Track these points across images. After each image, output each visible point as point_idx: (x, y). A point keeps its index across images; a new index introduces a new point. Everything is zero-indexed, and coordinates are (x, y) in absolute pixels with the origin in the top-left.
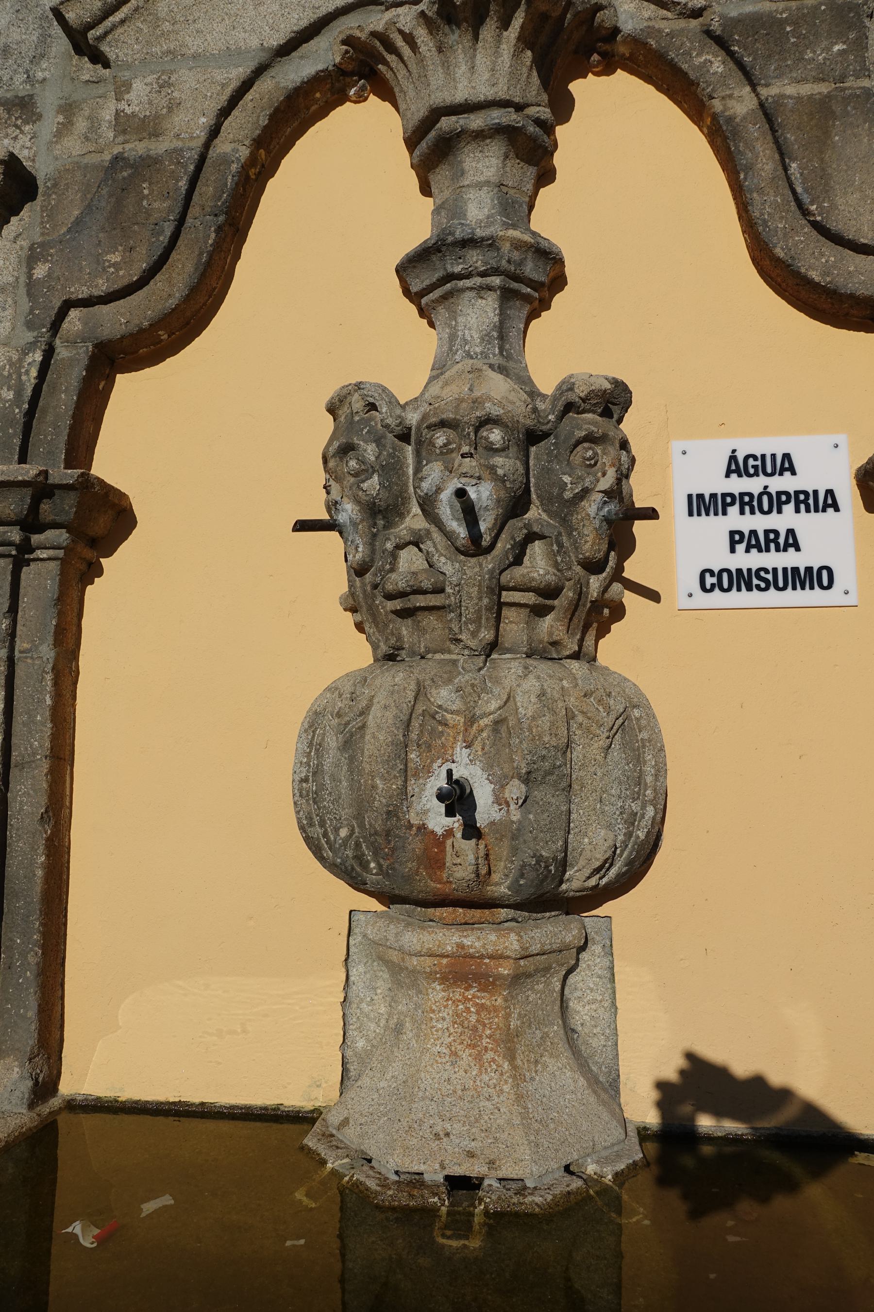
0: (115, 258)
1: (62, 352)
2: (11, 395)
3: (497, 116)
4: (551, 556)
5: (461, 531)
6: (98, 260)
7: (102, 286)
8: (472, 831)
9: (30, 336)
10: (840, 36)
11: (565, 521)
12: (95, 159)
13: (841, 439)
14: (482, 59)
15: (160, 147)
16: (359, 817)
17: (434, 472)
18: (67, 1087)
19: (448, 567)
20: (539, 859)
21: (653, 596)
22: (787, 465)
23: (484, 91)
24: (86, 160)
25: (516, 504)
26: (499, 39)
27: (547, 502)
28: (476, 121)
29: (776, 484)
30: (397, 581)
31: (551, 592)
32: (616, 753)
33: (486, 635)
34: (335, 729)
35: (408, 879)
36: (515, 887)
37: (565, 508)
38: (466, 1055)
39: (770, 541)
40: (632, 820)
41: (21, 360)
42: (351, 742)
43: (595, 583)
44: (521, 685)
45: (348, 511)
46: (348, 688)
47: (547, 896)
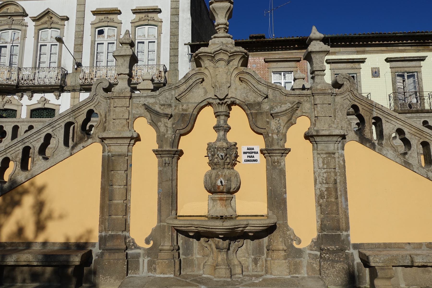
1: (176, 135)
3: (224, 113)
7: (181, 128)
8: (222, 185)
14: (222, 107)
15: (187, 113)
16: (211, 184)
17: (219, 152)
18: (178, 214)
29: (252, 151)
30: (215, 162)
31: (229, 163)
34: (208, 176)
37: (231, 155)
39: (251, 157)
42: (210, 177)
43: (234, 162)
44: (227, 172)
45: (210, 155)
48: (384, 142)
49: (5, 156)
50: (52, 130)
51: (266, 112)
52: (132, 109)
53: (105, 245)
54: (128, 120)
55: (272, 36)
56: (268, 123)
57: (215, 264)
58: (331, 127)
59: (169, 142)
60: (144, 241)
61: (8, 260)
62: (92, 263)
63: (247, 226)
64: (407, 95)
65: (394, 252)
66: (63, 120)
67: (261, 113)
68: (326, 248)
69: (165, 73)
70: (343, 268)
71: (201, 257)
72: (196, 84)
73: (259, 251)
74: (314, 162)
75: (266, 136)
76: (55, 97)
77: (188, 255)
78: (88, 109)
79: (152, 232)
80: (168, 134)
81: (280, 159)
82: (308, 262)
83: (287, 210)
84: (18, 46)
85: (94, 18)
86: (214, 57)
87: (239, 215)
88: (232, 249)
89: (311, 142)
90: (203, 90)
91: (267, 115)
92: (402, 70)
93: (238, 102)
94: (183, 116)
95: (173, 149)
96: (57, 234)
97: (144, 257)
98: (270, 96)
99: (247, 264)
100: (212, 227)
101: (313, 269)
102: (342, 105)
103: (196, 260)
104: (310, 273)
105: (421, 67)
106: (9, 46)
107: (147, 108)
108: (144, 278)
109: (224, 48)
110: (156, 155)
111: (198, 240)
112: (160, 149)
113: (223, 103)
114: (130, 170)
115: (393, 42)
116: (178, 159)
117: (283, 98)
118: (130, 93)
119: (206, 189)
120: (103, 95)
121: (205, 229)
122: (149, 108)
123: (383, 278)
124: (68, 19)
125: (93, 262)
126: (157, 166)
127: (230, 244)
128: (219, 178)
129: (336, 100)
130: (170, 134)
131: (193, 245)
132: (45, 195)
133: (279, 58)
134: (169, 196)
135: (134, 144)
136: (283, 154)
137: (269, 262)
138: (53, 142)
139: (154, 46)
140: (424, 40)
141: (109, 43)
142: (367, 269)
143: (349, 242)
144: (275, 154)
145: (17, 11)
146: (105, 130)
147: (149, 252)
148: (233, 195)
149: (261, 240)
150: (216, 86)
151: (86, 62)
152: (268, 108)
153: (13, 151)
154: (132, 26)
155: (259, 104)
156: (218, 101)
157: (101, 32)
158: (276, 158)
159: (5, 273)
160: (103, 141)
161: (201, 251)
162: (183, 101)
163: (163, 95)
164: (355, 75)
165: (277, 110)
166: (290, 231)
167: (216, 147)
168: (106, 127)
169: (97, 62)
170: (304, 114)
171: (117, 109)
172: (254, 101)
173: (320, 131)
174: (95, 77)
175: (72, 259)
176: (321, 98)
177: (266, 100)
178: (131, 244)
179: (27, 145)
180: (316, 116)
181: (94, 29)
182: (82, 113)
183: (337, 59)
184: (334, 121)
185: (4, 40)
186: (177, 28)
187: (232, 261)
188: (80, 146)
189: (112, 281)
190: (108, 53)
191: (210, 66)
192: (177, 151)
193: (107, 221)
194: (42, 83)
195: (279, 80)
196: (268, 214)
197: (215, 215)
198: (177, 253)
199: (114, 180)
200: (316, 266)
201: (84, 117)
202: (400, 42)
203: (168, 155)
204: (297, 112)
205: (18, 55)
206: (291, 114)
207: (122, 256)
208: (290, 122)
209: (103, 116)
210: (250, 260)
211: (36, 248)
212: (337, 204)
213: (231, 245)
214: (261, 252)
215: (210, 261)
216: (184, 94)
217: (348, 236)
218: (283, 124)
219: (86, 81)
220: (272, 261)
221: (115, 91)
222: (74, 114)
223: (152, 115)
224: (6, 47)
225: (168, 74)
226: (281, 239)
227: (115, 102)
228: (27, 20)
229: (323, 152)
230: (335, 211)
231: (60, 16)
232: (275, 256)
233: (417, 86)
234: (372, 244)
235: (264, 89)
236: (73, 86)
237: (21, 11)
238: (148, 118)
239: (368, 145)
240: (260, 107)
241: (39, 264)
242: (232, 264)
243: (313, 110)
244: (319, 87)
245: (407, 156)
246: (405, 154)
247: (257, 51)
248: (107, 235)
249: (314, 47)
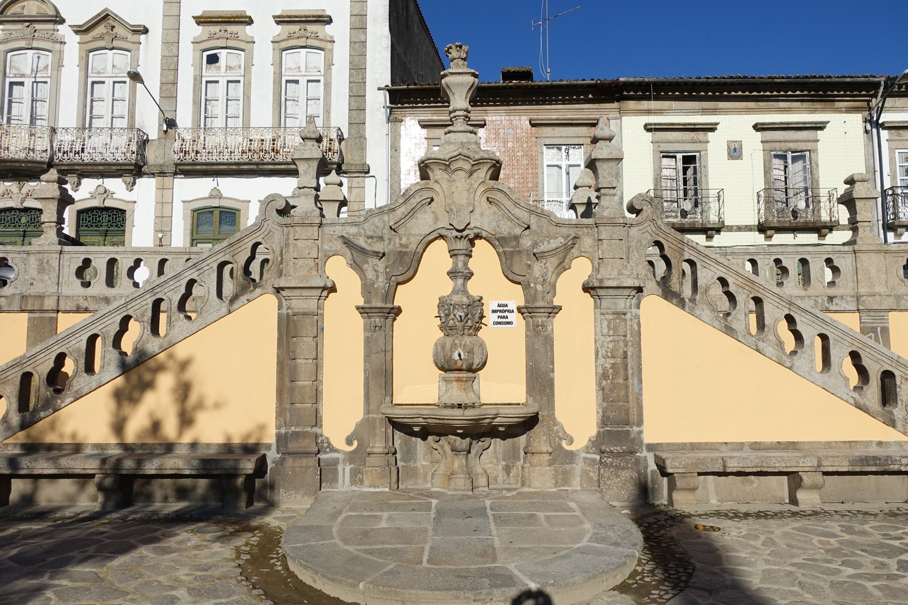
3: (464, 252)
15: (408, 250)
17: (456, 311)
22: (507, 306)
28: (460, 252)
29: (505, 308)
30: (450, 325)
34: (440, 347)
37: (473, 315)
42: (443, 347)
44: (467, 340)
45: (442, 315)
47: (470, 370)
48: (698, 297)
49: (125, 314)
50: (197, 273)
52: (322, 242)
53: (286, 447)
55: (544, 76)
56: (529, 266)
58: (622, 274)
60: (344, 442)
61: (147, 467)
62: (266, 473)
63: (496, 416)
64: (791, 193)
65: (702, 455)
66: (215, 258)
69: (340, 143)
70: (631, 477)
72: (421, 205)
73: (512, 455)
75: (526, 287)
76: (125, 186)
77: (410, 461)
79: (355, 429)
84: (46, 82)
85: (199, 31)
86: (449, 166)
90: (432, 216)
91: (528, 255)
92: (784, 146)
93: (484, 234)
95: (383, 305)
96: (211, 431)
98: (533, 227)
99: (495, 473)
101: (590, 479)
102: (639, 241)
104: (585, 485)
105: (818, 141)
106: (28, 82)
107: (347, 242)
108: (347, 492)
109: (465, 152)
112: (367, 305)
113: (462, 237)
115: (768, 93)
116: (394, 319)
119: (437, 365)
121: (438, 421)
123: (683, 489)
124: (146, 31)
127: (471, 444)
128: (456, 349)
129: (631, 233)
131: (416, 447)
132: (191, 374)
133: (557, 119)
134: (380, 375)
135: (327, 297)
137: (526, 470)
138: (196, 290)
139: (318, 90)
140: (825, 92)
142: (665, 479)
143: (641, 442)
145: (42, 11)
146: (281, 275)
147: (351, 457)
150: (451, 210)
151: (184, 119)
153: (138, 307)
154: (274, 49)
155: (517, 238)
156: (455, 233)
157: (213, 60)
158: (540, 320)
159: (136, 487)
160: (278, 292)
162: (401, 231)
164: (697, 154)
165: (544, 247)
168: (282, 271)
169: (206, 117)
171: (299, 243)
172: (509, 233)
174: (204, 148)
175: (242, 466)
178: (325, 445)
179: (158, 296)
181: (199, 53)
182: (244, 247)
183: (666, 124)
185: (18, 69)
186: (364, 55)
188: (243, 299)
189: (299, 497)
190: (227, 100)
191: (443, 178)
192: (393, 308)
194: (98, 159)
195: (558, 160)
197: (449, 402)
199: (298, 351)
200: (594, 475)
202: (782, 93)
204: (573, 250)
205: (48, 100)
207: (312, 462)
209: (278, 252)
210: (500, 467)
211: (182, 451)
212: (627, 387)
214: (516, 457)
215: (442, 469)
217: (641, 432)
218: (551, 269)
219: (187, 157)
220: (531, 468)
222: (232, 249)
224: (21, 84)
225: (347, 146)
226: (544, 438)
228: (64, 31)
231: (132, 26)
233: (809, 176)
234: (674, 444)
235: (523, 215)
236: (161, 166)
237: (51, 12)
239: (674, 301)
240: (518, 243)
241: (193, 473)
244: (606, 214)
245: (729, 318)
246: (728, 314)
247: (516, 104)
249: (601, 151)
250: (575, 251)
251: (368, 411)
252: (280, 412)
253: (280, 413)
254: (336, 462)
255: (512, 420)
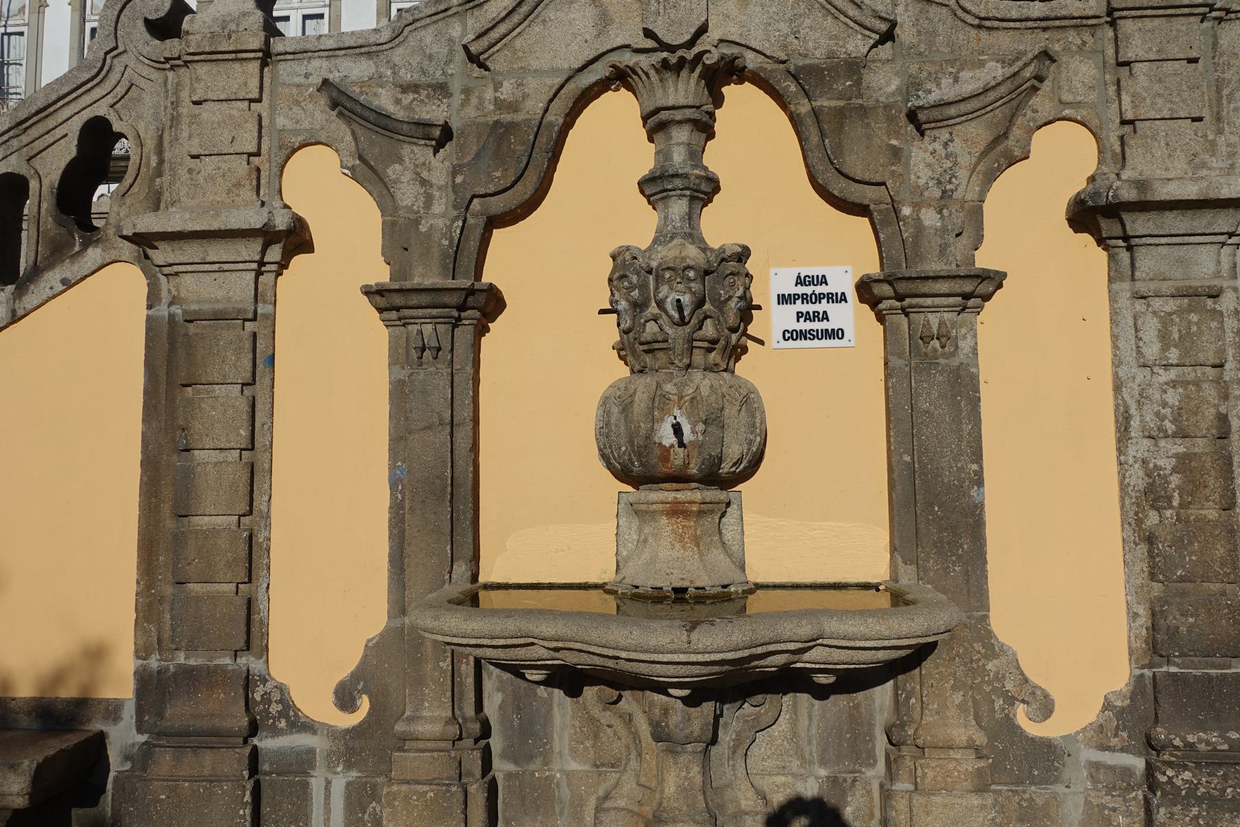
0: (498, 174)
1: (471, 221)
2: (447, 243)
3: (689, 113)
4: (715, 326)
5: (676, 316)
6: (489, 175)
8: (681, 444)
9: (455, 213)
10: (850, 78)
11: (721, 310)
12: (482, 120)
13: (849, 268)
15: (519, 117)
16: (631, 442)
17: (664, 290)
19: (669, 330)
20: (711, 456)
21: (762, 343)
23: (682, 101)
24: (478, 120)
25: (700, 303)
26: (689, 77)
27: (713, 302)
28: (678, 115)
29: (819, 289)
30: (646, 336)
31: (714, 342)
32: (743, 413)
33: (686, 361)
34: (617, 405)
35: (654, 466)
36: (700, 470)
37: (721, 304)
38: (678, 546)
39: (816, 317)
40: (750, 443)
41: (451, 225)
42: (626, 409)
43: (734, 337)
44: (702, 382)
45: (623, 305)
46: (623, 385)
51: (887, 107)
52: (273, 108)
54: (255, 160)
56: (896, 153)
57: (647, 810)
58: (1204, 165)
59: (436, 253)
63: (812, 642)
67: (863, 111)
68: (1177, 742)
71: (587, 767)
74: (1115, 338)
77: (530, 758)
78: (87, 115)
79: (365, 657)
80: (435, 216)
81: (954, 324)
82: (1087, 802)
83: (985, 562)
84: (21, 34)
87: (759, 581)
88: (725, 737)
89: (1100, 241)
90: (591, 12)
91: (890, 119)
93: (751, 61)
94: (500, 132)
95: (450, 283)
97: (331, 768)
98: (905, 33)
100: (633, 655)
103: (564, 784)
107: (340, 100)
110: (381, 310)
111: (574, 691)
113: (682, 60)
114: (267, 381)
116: (482, 330)
117: (968, 38)
118: (262, 34)
119: (609, 466)
120: (146, 50)
122: (344, 100)
125: (109, 786)
126: (386, 361)
127: (717, 718)
128: (665, 411)
129: (1223, 42)
130: (440, 217)
134: (439, 496)
135: (283, 265)
136: (967, 296)
137: (901, 804)
141: (305, 17)
144: (929, 301)
147: (352, 747)
148: (731, 494)
149: (860, 696)
152: (893, 87)
155: (855, 67)
158: (934, 320)
161: (588, 744)
162: (498, 63)
163: (412, 42)
166: (1003, 659)
167: (654, 264)
170: (1067, 112)
172: (831, 55)
173: (1157, 185)
176: (1152, 31)
177: (886, 50)
178: (275, 708)
180: (1129, 116)
182: (58, 133)
184: (1213, 144)
187: (729, 794)
188: (53, 278)
192: (471, 292)
193: (167, 607)
196: (895, 578)
197: (648, 582)
198: (477, 754)
199: (197, 426)
201: (66, 152)
203: (434, 312)
204: (1035, 101)
205: (24, 62)
206: (1006, 110)
207: (232, 762)
208: (1001, 148)
209: (150, 144)
213: (722, 721)
214: (859, 752)
216: (502, 29)
218: (965, 160)
220: (918, 800)
221: (196, 26)
222: (25, 139)
223: (360, 132)
226: (958, 698)
227: (198, 80)
229: (1166, 287)
230: (1223, 565)
232: (930, 774)
238: (342, 146)
240: (858, 82)
242: (731, 809)
243: (1112, 89)
248: (167, 669)
250: (1041, 103)
251: (399, 606)
252: (148, 608)
253: (147, 609)
254: (303, 762)
255: (868, 656)
